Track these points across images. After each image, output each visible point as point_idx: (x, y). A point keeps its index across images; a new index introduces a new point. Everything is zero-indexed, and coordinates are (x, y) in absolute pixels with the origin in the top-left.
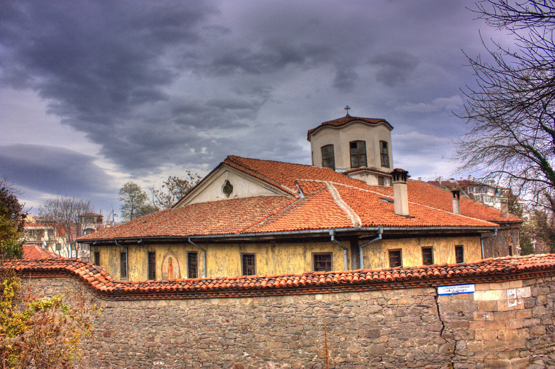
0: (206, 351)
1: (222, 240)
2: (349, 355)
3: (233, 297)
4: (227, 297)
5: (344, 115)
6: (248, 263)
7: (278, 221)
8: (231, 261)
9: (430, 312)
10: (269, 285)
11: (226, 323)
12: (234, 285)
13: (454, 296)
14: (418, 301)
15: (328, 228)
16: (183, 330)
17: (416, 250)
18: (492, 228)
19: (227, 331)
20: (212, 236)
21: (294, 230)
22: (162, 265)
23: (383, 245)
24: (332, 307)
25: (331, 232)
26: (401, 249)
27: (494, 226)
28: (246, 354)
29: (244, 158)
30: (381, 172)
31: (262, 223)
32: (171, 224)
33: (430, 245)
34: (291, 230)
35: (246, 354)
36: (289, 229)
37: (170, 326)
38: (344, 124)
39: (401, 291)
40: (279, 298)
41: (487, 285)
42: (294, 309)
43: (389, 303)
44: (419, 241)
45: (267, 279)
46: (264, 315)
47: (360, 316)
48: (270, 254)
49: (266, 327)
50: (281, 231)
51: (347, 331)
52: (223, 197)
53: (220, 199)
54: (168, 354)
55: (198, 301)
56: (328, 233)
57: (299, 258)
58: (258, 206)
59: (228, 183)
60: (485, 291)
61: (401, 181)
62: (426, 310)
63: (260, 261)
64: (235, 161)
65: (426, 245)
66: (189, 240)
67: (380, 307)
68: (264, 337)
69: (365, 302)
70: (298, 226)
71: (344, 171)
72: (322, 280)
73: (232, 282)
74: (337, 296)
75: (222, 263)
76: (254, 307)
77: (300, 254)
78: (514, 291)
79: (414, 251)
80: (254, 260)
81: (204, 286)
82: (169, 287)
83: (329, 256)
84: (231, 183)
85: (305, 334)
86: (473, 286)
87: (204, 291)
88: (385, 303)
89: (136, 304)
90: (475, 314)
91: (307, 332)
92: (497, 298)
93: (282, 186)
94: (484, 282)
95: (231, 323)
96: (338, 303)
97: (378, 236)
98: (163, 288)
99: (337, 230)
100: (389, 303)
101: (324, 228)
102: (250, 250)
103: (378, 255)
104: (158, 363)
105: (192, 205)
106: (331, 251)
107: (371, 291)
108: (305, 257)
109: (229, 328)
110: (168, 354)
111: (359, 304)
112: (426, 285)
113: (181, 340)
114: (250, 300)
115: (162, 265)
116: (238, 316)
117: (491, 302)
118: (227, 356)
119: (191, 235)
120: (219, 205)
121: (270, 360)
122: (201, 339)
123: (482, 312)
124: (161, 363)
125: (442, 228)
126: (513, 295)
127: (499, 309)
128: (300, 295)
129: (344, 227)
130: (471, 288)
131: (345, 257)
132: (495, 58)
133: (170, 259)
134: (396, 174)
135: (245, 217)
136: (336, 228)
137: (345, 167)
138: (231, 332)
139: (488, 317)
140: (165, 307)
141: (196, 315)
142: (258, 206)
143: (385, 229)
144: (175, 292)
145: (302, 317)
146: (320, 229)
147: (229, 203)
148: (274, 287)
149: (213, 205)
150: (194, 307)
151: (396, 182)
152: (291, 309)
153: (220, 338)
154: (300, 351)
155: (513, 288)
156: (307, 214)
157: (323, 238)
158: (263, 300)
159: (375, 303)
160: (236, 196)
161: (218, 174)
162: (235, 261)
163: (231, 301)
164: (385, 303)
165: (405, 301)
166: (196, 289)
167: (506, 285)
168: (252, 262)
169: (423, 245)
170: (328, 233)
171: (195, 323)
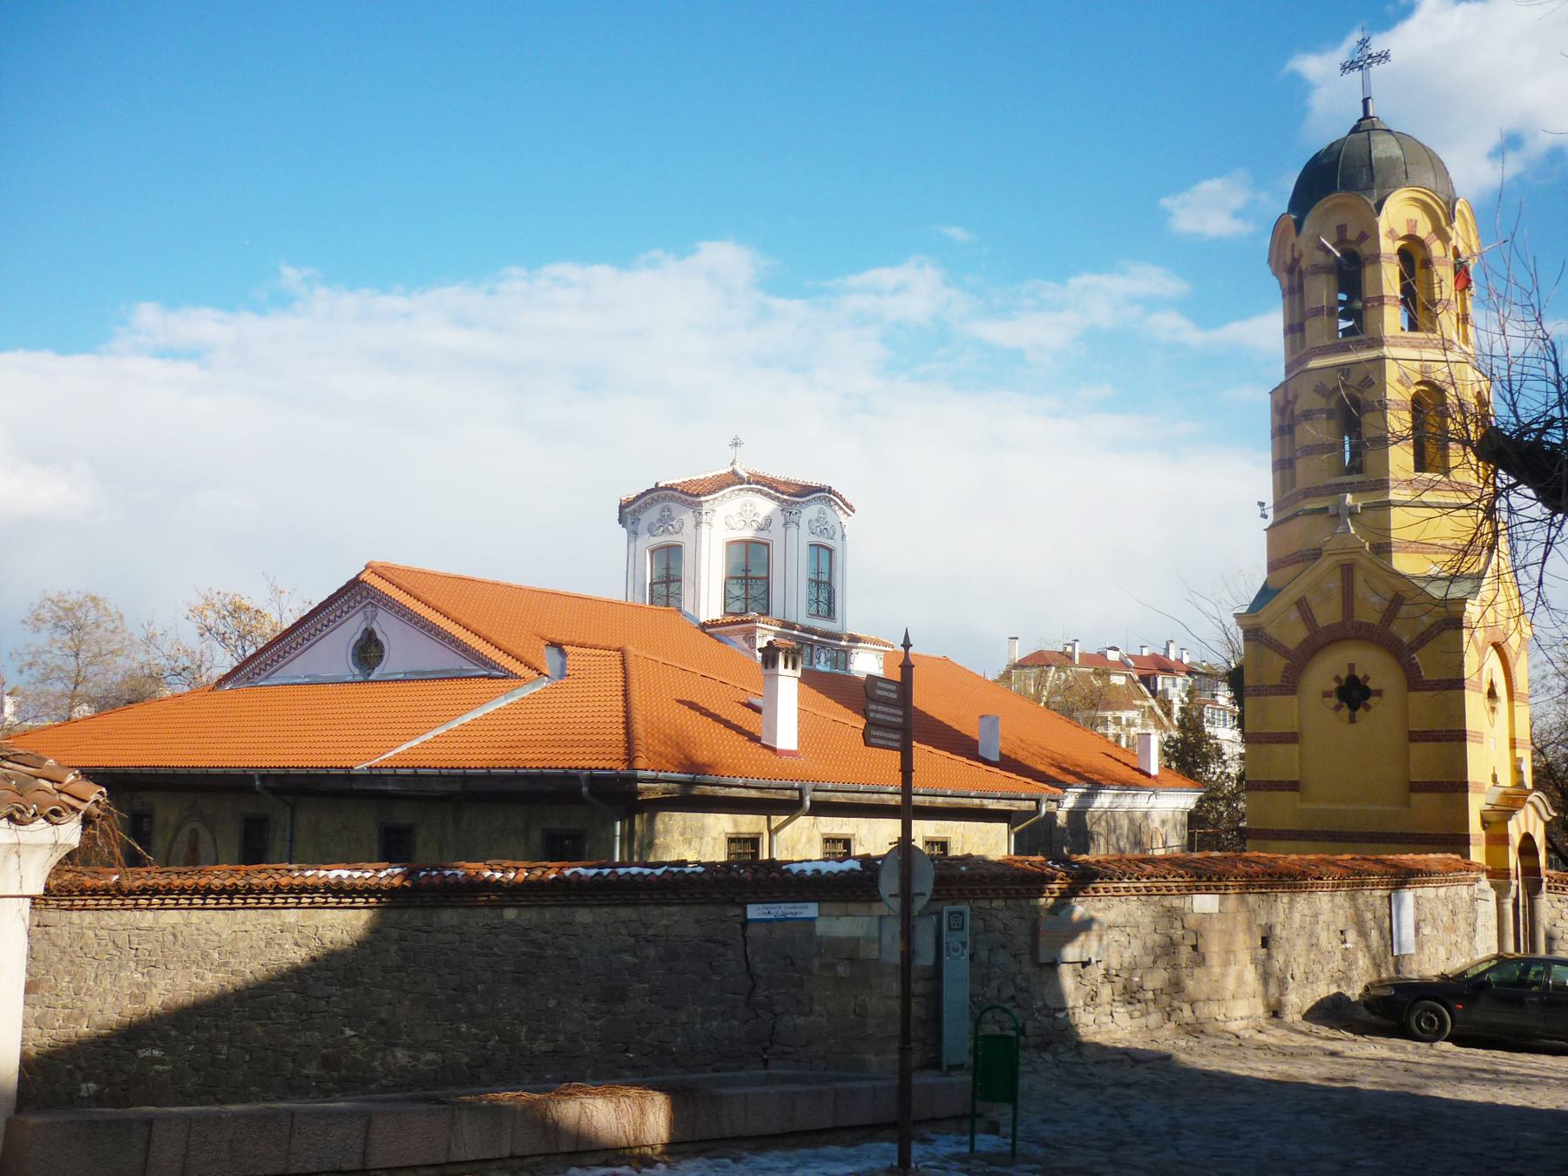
2: (561, 1038)
9: (730, 955)
22: (170, 850)
24: (533, 935)
35: (348, 1032)
39: (674, 909)
46: (394, 948)
60: (838, 917)
67: (632, 940)
89: (112, 919)
90: (816, 963)
92: (860, 933)
100: (651, 932)
104: (148, 1053)
115: (170, 850)
117: (849, 940)
121: (397, 1045)
124: (156, 1053)
127: (862, 955)
130: (810, 910)
132: (1128, 1086)
133: (195, 833)
139: (842, 970)
153: (294, 996)
159: (624, 932)
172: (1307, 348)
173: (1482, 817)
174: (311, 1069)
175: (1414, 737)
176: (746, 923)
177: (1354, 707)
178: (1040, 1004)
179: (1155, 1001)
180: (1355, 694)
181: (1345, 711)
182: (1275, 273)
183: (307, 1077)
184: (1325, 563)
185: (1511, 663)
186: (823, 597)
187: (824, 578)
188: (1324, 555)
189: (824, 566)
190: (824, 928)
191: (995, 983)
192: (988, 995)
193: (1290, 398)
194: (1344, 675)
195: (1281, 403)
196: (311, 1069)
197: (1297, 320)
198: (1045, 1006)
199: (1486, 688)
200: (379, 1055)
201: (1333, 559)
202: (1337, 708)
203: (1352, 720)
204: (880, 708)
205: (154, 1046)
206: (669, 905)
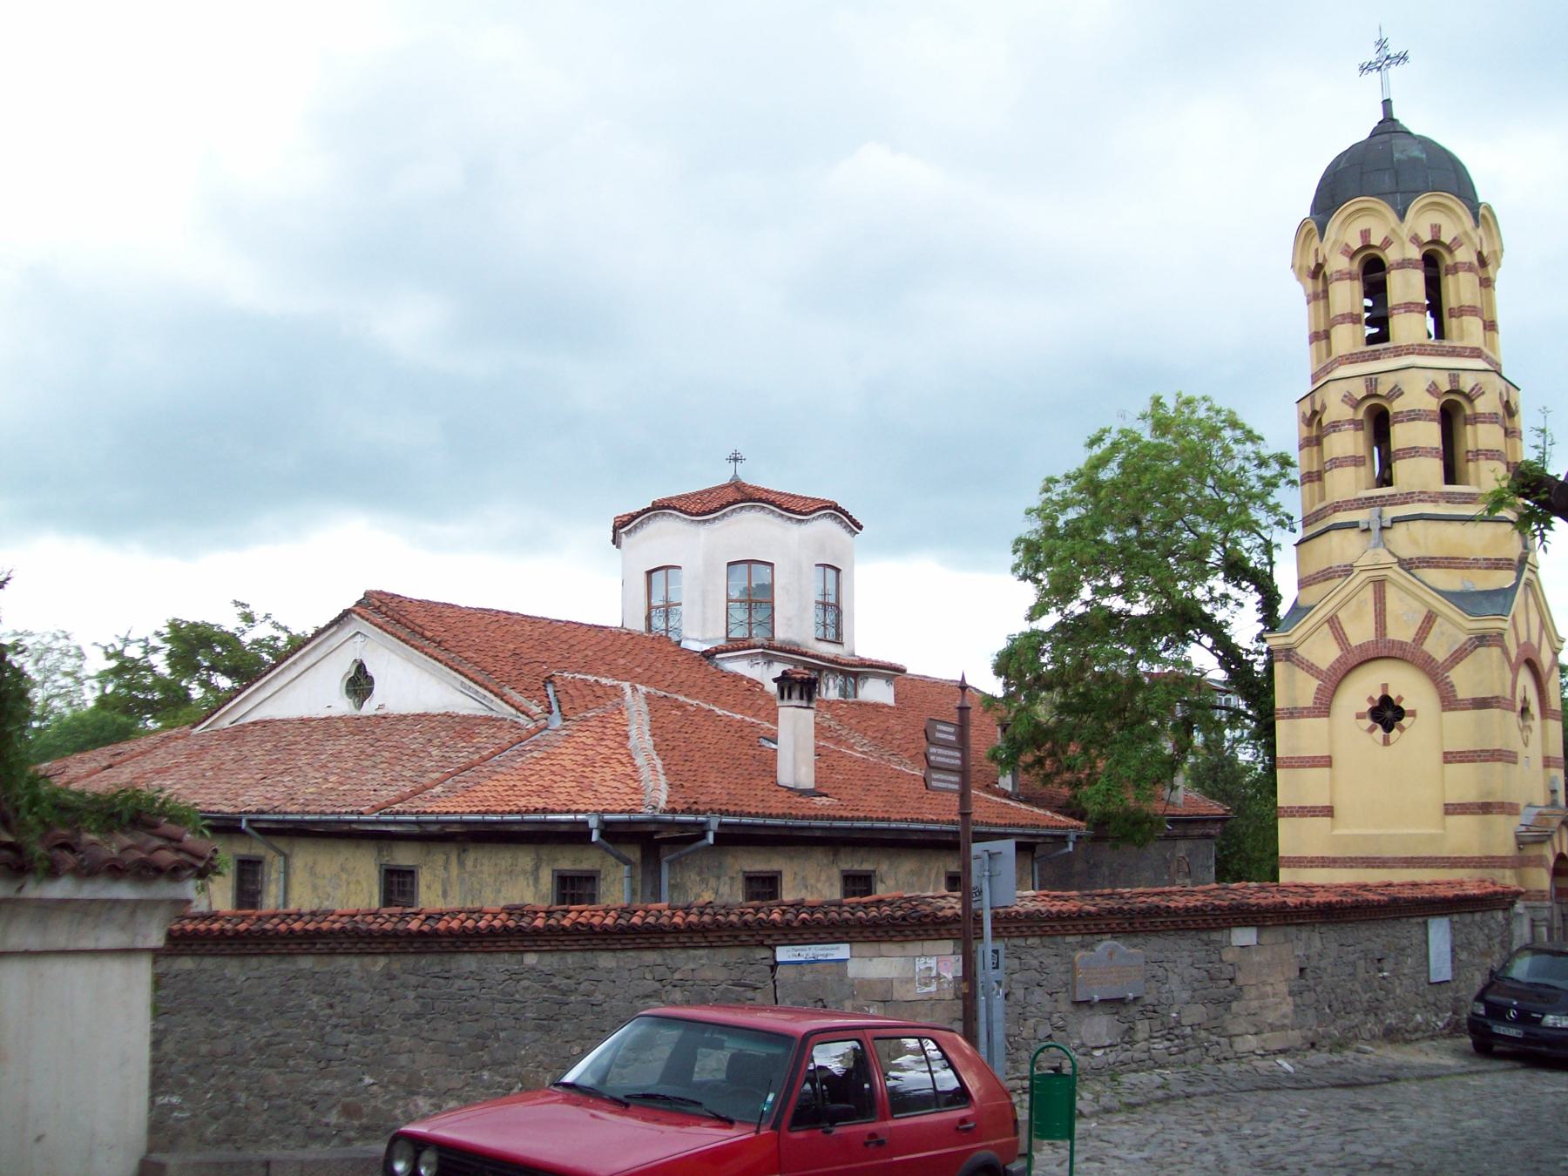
0: (280, 1073)
1: (334, 828)
3: (346, 954)
4: (332, 953)
5: (725, 479)
6: (398, 884)
7: (478, 788)
8: (352, 886)
10: (425, 928)
11: (328, 1011)
12: (349, 926)
13: (808, 968)
14: (736, 974)
15: (586, 812)
16: (229, 1025)
17: (823, 878)
18: (1058, 832)
19: (328, 1029)
20: (307, 818)
21: (510, 813)
23: (729, 860)
24: (556, 981)
25: (593, 822)
26: (780, 873)
27: (1067, 828)
28: (368, 1080)
29: (411, 601)
30: (813, 657)
31: (438, 789)
32: (193, 776)
33: (867, 867)
34: (503, 813)
35: (368, 1080)
36: (500, 809)
37: (199, 1015)
38: (715, 511)
39: (701, 952)
40: (446, 958)
41: (876, 945)
42: (477, 984)
43: (677, 976)
44: (835, 855)
45: (422, 917)
46: (411, 995)
47: (614, 1002)
48: (454, 869)
49: (414, 1021)
50: (478, 812)
51: (587, 1033)
52: (343, 706)
53: (335, 712)
54: (192, 1081)
55: (267, 961)
56: (586, 823)
57: (522, 881)
58: (436, 742)
59: (360, 667)
60: (871, 958)
61: (797, 703)
62: (750, 994)
63: (429, 887)
64: (384, 609)
65: (856, 867)
66: (244, 825)
67: (658, 985)
68: (408, 1042)
69: (626, 974)
70: (522, 802)
71: (706, 647)
72: (539, 923)
73: (345, 919)
74: (570, 959)
75: (329, 889)
76: (392, 977)
77: (524, 872)
78: (932, 962)
79: (818, 880)
80: (412, 884)
81: (283, 927)
82: (202, 927)
83: (591, 878)
84: (370, 670)
85: (498, 1039)
86: (847, 946)
87: (283, 938)
88: (668, 975)
91: (502, 1035)
93: (506, 690)
94: (867, 940)
95: (339, 1010)
96: (571, 973)
97: (703, 836)
98: (190, 927)
99: (607, 817)
100: (677, 976)
101: (577, 812)
102: (404, 857)
103: (713, 882)
104: (166, 1100)
105: (255, 723)
106: (597, 867)
107: (638, 949)
108: (537, 880)
109: (334, 1021)
110: (192, 1081)
111: (613, 976)
112: (752, 941)
113: (223, 1046)
114: (382, 961)
116: (356, 995)
117: (882, 981)
118: (326, 1085)
119: (250, 812)
120: (333, 731)
121: (418, 1094)
122: (269, 1044)
123: (861, 1001)
124: (175, 1100)
125: (893, 825)
126: (930, 969)
127: (896, 996)
128: (490, 952)
129: (622, 812)
130: (842, 951)
131: (626, 881)
134: (786, 684)
135: (398, 768)
136: (605, 811)
137: (709, 635)
138: (338, 1031)
140: (190, 972)
141: (261, 991)
142: (436, 742)
143: (725, 820)
144: (216, 938)
145: (493, 999)
146: (568, 812)
147: (358, 726)
148: (435, 933)
149: (314, 729)
150: (257, 974)
151: (786, 702)
152: (470, 983)
153: (311, 1044)
154: (486, 1075)
155: (931, 956)
156: (553, 773)
157: (575, 836)
158: (410, 961)
159: (648, 976)
160: (381, 707)
161: (335, 641)
162: (365, 885)
163: (342, 962)
164: (668, 975)
165: (708, 974)
166: (265, 931)
167: (913, 948)
168: (408, 888)
169: (846, 867)
170: (586, 823)
171: (258, 1010)
172: (1333, 356)
173: (1517, 837)
174: (333, 1118)
175: (1449, 757)
176: (774, 966)
177: (1388, 728)
178: (1077, 1042)
179: (1193, 1037)
180: (1389, 714)
181: (1379, 732)
182: (1299, 279)
183: (327, 1125)
184: (1358, 579)
185: (1544, 679)
186: (830, 618)
187: (832, 600)
188: (1356, 571)
189: (831, 587)
190: (855, 969)
191: (1031, 1022)
192: (1024, 1035)
193: (1318, 408)
194: (1377, 696)
195: (1308, 414)
196: (333, 1118)
197: (1322, 328)
198: (1083, 1045)
199: (1519, 707)
200: (400, 1103)
201: (1364, 575)
202: (1371, 730)
203: (1386, 742)
204: (940, 751)
205: (173, 1093)
206: (694, 948)
